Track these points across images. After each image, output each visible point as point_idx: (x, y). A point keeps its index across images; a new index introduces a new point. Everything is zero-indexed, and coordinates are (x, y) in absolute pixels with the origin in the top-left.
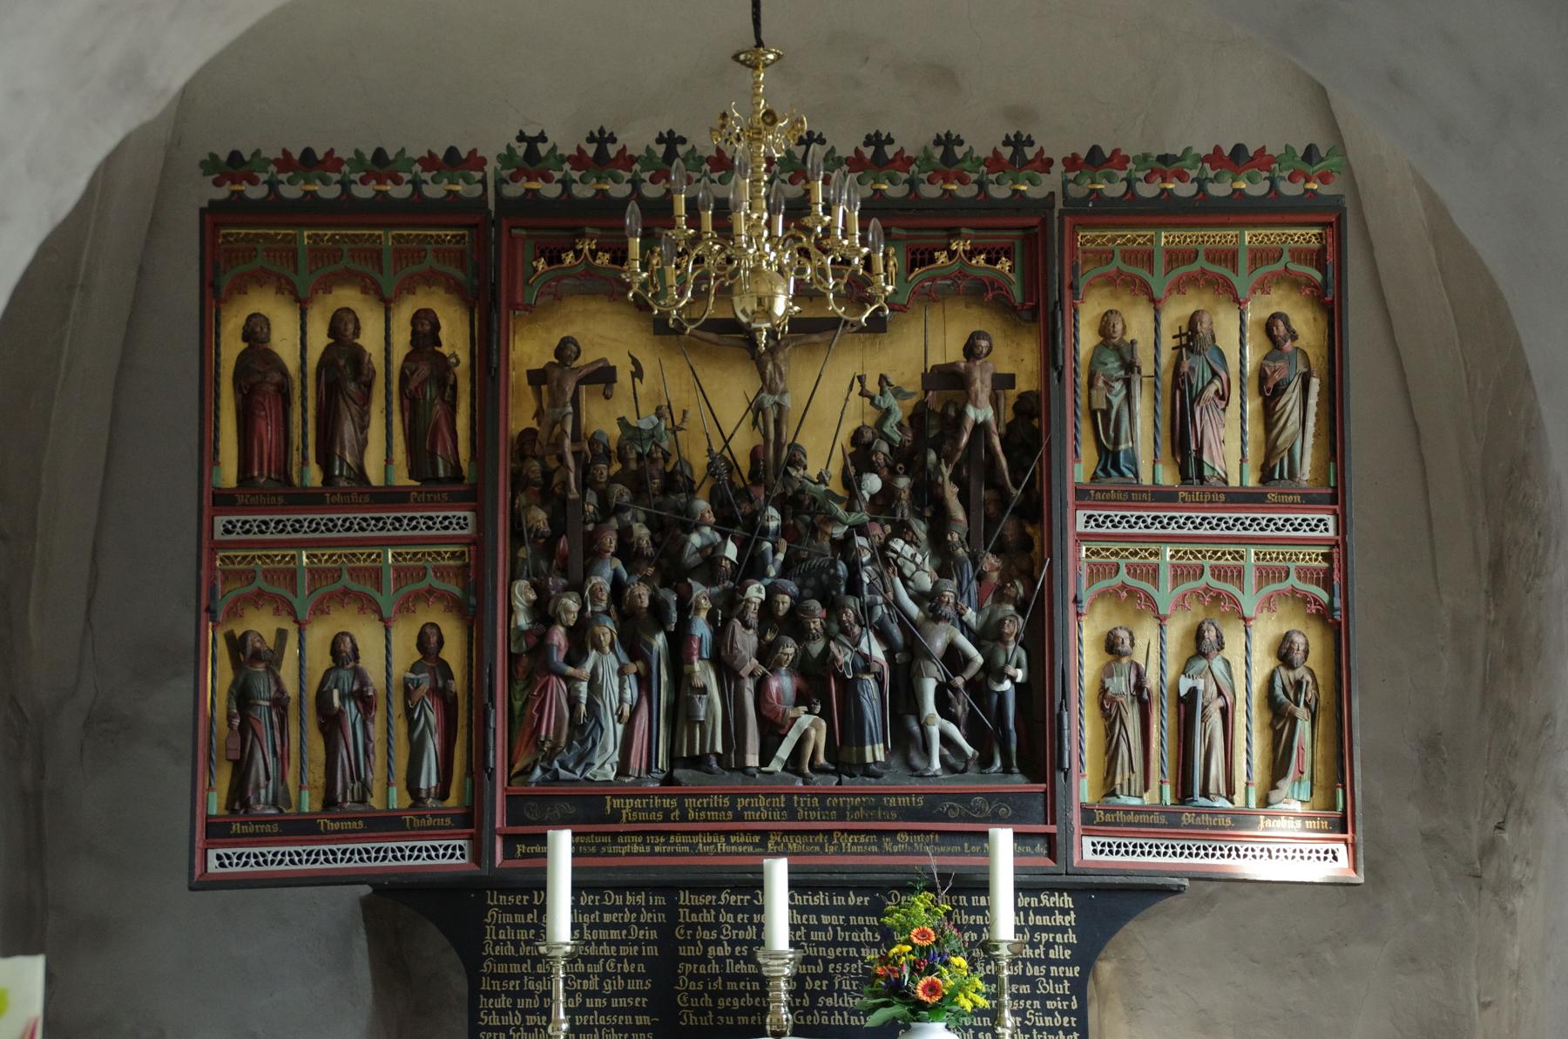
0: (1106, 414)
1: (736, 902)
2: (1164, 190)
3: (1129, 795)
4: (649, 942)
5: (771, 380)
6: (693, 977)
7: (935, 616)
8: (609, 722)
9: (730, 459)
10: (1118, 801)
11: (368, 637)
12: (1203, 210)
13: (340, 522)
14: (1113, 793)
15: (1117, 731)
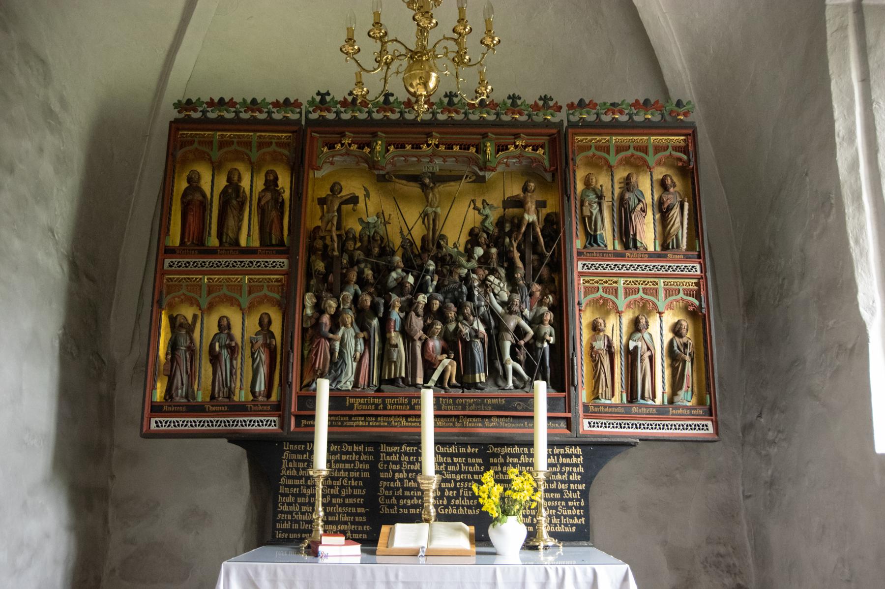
0: (590, 218)
1: (410, 450)
2: (613, 118)
3: (606, 399)
4: (365, 470)
5: (431, 201)
6: (387, 488)
7: (511, 312)
8: (349, 361)
9: (412, 240)
10: (600, 402)
11: (235, 318)
12: (631, 127)
13: (223, 263)
14: (598, 398)
15: (599, 367)
